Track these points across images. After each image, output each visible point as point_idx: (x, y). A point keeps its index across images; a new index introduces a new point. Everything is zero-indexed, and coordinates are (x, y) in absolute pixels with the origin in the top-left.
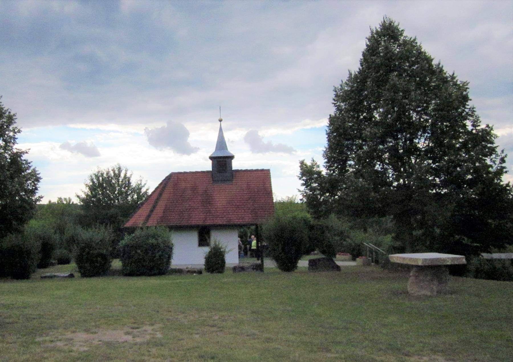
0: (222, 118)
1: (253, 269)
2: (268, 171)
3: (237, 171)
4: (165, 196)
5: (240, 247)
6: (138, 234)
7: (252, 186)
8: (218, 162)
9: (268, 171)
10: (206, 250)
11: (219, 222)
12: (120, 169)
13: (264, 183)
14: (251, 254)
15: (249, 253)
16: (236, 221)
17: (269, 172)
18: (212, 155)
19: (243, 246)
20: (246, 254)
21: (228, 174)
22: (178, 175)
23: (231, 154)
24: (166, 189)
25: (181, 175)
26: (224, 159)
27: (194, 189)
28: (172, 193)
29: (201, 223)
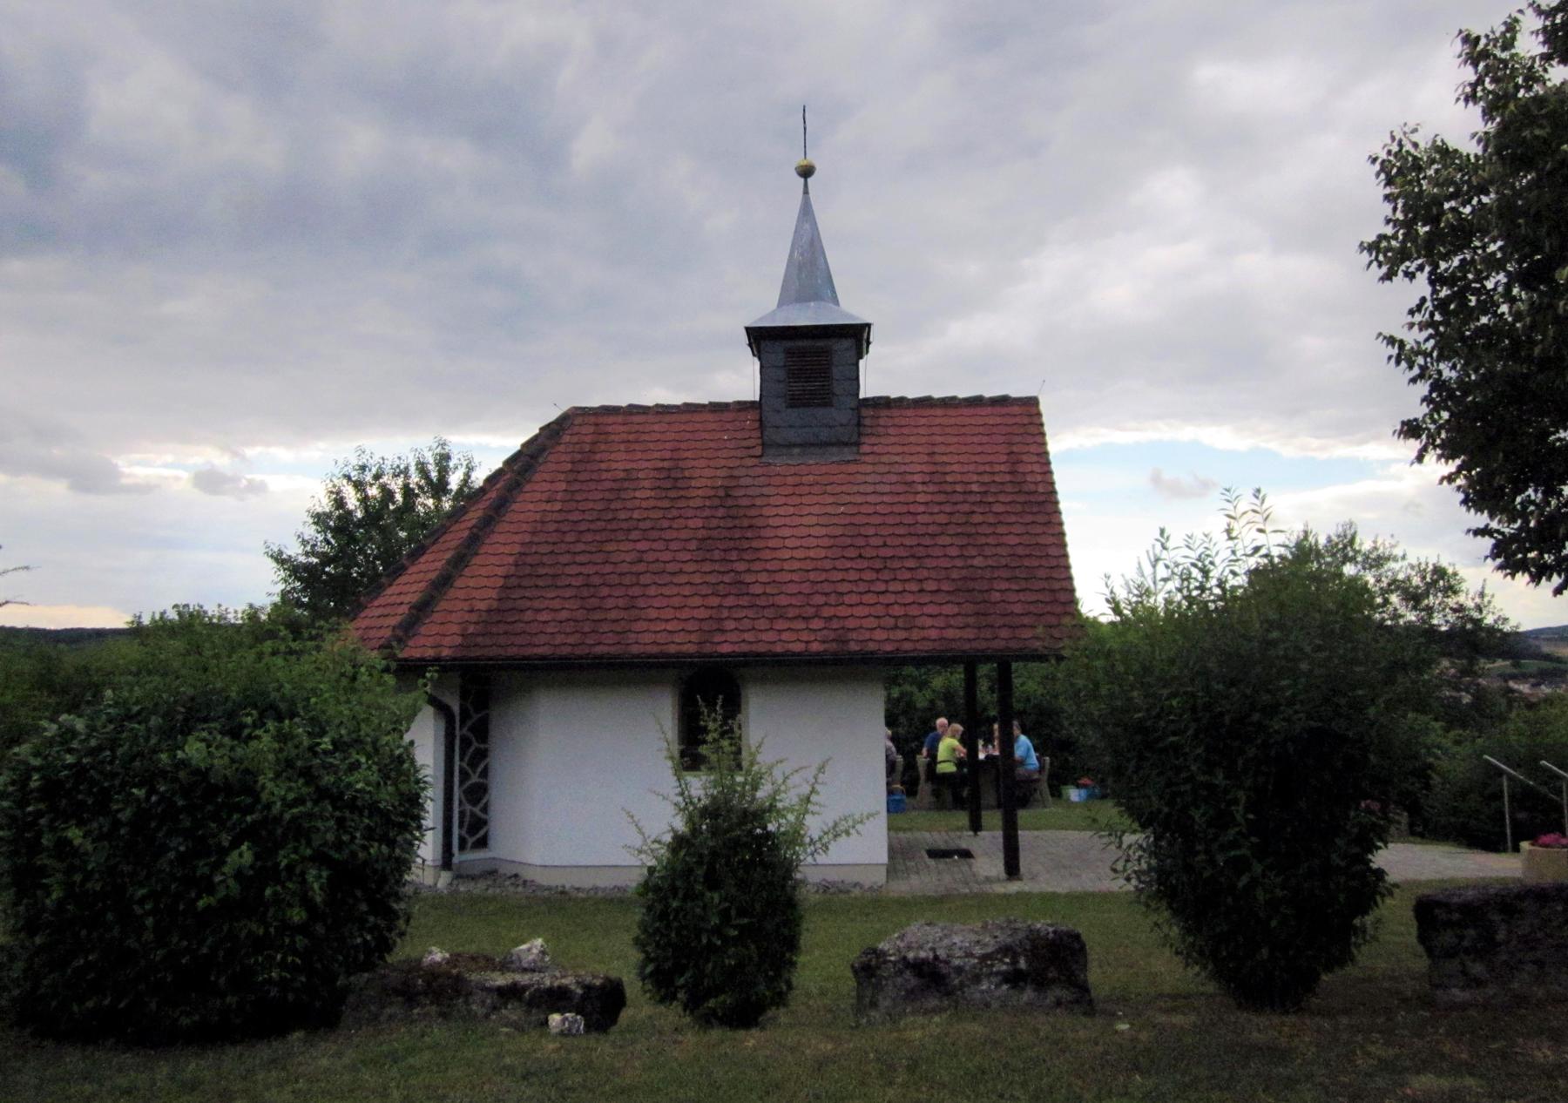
0: (812, 159)
1: (1015, 979)
2: (1031, 403)
3: (883, 404)
4: (527, 507)
5: (891, 767)
6: (1096, 713)
7: (955, 468)
8: (789, 353)
9: (1031, 403)
10: (699, 786)
11: (793, 639)
12: (443, 460)
13: (1014, 460)
14: (936, 794)
15: (925, 788)
16: (882, 640)
17: (1033, 411)
18: (761, 319)
19: (900, 758)
20: (911, 788)
21: (840, 415)
22: (601, 420)
23: (852, 317)
24: (537, 477)
25: (611, 419)
26: (820, 343)
27: (672, 480)
28: (559, 496)
29: (684, 643)
